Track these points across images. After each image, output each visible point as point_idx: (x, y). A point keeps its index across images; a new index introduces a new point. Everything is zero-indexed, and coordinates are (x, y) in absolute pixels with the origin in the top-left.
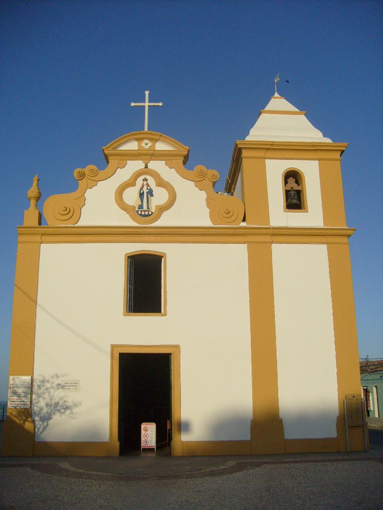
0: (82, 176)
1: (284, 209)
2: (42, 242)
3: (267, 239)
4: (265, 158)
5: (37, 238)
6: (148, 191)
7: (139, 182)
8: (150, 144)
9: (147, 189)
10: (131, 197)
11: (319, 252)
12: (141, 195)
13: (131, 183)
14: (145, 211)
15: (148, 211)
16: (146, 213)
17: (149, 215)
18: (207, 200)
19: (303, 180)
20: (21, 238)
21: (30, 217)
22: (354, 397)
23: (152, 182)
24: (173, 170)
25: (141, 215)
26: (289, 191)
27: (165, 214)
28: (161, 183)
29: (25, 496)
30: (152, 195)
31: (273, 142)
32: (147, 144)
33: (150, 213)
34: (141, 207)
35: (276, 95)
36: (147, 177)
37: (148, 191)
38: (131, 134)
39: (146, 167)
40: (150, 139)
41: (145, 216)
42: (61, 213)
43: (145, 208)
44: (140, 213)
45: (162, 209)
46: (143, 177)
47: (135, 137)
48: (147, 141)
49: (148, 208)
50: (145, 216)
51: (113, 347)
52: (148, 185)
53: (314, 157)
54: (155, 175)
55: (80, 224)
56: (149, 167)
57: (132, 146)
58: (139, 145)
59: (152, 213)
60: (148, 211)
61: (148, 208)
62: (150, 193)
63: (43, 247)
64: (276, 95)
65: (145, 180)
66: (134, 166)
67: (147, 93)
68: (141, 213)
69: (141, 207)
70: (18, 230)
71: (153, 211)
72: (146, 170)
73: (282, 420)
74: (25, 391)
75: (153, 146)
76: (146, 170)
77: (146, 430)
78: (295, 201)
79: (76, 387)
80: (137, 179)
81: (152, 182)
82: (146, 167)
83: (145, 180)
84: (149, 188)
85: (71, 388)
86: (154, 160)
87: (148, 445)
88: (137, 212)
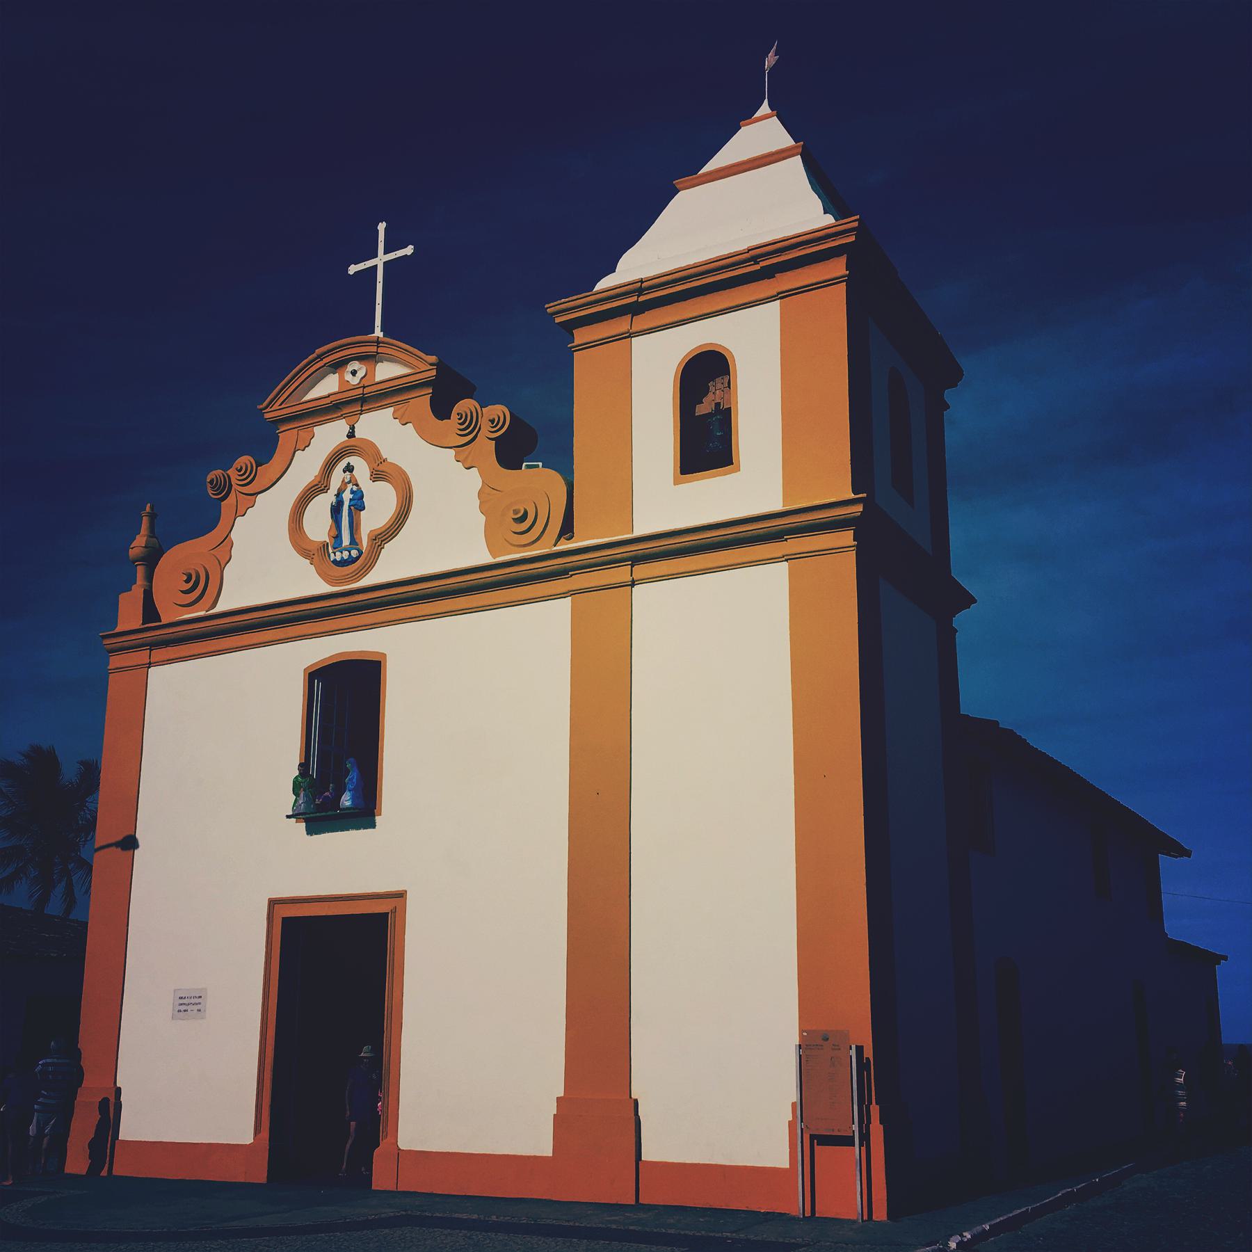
0: (224, 488)
2: (150, 665)
3: (621, 574)
5: (142, 656)
7: (338, 476)
10: (318, 524)
11: (147, 517)
20: (116, 661)
21: (129, 614)
23: (362, 469)
31: (642, 281)
32: (354, 373)
34: (338, 537)
35: (765, 108)
38: (314, 355)
39: (351, 435)
40: (361, 358)
43: (346, 541)
47: (325, 361)
48: (355, 365)
54: (369, 451)
55: (221, 607)
57: (328, 386)
62: (358, 503)
63: (157, 675)
64: (765, 108)
66: (330, 435)
67: (382, 227)
70: (106, 642)
79: (199, 1007)
82: (351, 435)
83: (349, 468)
85: (189, 1008)
86: (370, 410)
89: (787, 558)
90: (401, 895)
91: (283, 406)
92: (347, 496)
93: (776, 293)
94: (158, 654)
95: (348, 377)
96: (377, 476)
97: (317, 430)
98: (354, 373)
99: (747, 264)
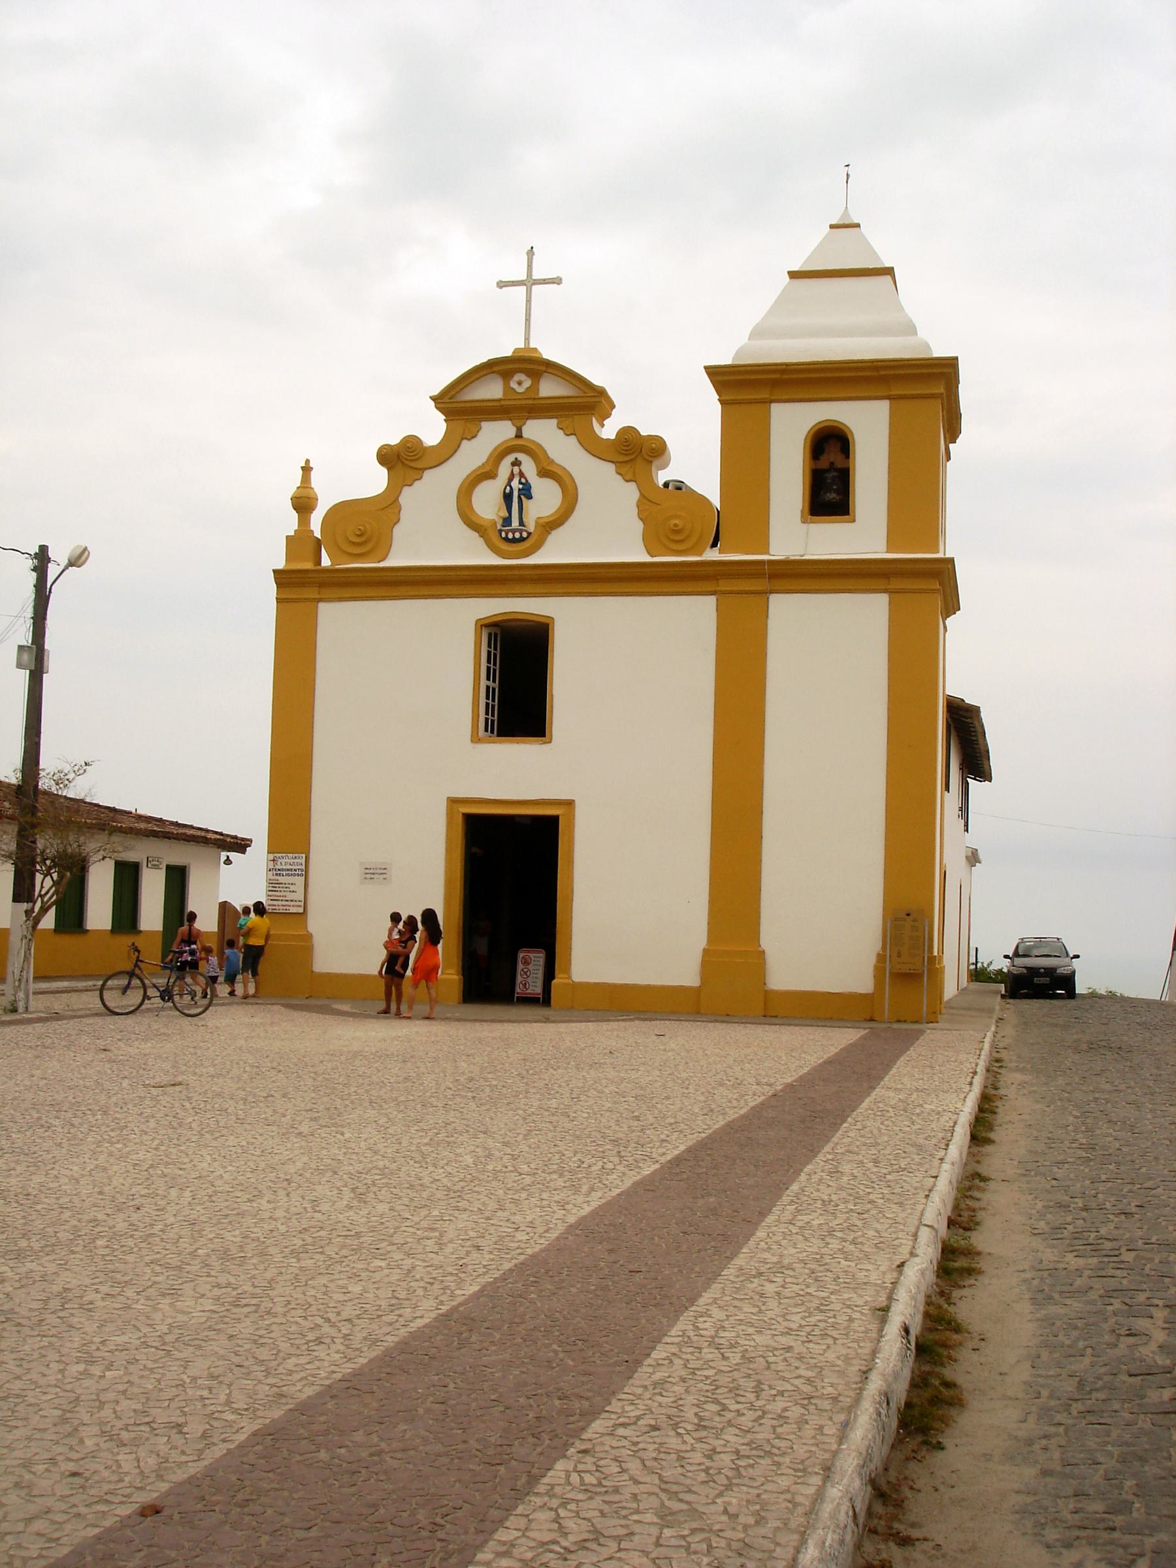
1: (802, 516)
4: (771, 402)
6: (521, 486)
7: (505, 469)
8: (527, 383)
9: (520, 483)
12: (508, 498)
13: (486, 474)
14: (514, 531)
15: (521, 532)
16: (517, 535)
17: (522, 540)
18: (639, 505)
19: (808, 444)
22: (908, 915)
23: (529, 467)
24: (573, 439)
25: (506, 539)
26: (824, 471)
27: (555, 537)
28: (548, 471)
29: (585, 1189)
30: (530, 497)
32: (520, 383)
33: (525, 535)
34: (507, 521)
36: (521, 457)
37: (521, 486)
39: (519, 435)
41: (514, 541)
42: (351, 539)
43: (515, 523)
44: (503, 535)
45: (551, 525)
46: (510, 458)
49: (521, 523)
50: (514, 541)
51: (453, 802)
52: (521, 474)
53: (879, 394)
54: (535, 452)
55: (391, 562)
56: (524, 435)
58: (507, 389)
59: (529, 534)
60: (521, 532)
61: (521, 523)
62: (526, 491)
65: (516, 463)
68: (507, 534)
69: (507, 521)
71: (531, 529)
72: (518, 446)
73: (764, 952)
74: (994, 1116)
75: (534, 387)
76: (518, 446)
77: (526, 962)
78: (831, 496)
79: (384, 876)
80: (499, 463)
81: (529, 467)
82: (519, 435)
83: (516, 463)
84: (523, 480)
85: (375, 876)
87: (529, 991)
88: (500, 531)
89: (888, 398)
90: (570, 804)
91: (190, 1342)
92: (515, 484)
93: (979, 1240)
94: (326, 593)
95: (513, 385)
96: (544, 473)
97: (484, 425)
98: (520, 383)
99: (892, 372)
